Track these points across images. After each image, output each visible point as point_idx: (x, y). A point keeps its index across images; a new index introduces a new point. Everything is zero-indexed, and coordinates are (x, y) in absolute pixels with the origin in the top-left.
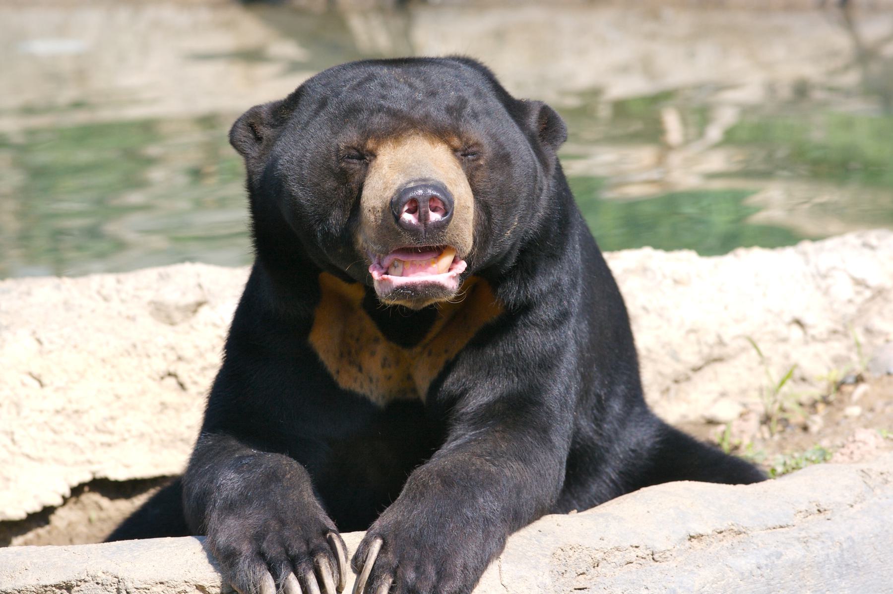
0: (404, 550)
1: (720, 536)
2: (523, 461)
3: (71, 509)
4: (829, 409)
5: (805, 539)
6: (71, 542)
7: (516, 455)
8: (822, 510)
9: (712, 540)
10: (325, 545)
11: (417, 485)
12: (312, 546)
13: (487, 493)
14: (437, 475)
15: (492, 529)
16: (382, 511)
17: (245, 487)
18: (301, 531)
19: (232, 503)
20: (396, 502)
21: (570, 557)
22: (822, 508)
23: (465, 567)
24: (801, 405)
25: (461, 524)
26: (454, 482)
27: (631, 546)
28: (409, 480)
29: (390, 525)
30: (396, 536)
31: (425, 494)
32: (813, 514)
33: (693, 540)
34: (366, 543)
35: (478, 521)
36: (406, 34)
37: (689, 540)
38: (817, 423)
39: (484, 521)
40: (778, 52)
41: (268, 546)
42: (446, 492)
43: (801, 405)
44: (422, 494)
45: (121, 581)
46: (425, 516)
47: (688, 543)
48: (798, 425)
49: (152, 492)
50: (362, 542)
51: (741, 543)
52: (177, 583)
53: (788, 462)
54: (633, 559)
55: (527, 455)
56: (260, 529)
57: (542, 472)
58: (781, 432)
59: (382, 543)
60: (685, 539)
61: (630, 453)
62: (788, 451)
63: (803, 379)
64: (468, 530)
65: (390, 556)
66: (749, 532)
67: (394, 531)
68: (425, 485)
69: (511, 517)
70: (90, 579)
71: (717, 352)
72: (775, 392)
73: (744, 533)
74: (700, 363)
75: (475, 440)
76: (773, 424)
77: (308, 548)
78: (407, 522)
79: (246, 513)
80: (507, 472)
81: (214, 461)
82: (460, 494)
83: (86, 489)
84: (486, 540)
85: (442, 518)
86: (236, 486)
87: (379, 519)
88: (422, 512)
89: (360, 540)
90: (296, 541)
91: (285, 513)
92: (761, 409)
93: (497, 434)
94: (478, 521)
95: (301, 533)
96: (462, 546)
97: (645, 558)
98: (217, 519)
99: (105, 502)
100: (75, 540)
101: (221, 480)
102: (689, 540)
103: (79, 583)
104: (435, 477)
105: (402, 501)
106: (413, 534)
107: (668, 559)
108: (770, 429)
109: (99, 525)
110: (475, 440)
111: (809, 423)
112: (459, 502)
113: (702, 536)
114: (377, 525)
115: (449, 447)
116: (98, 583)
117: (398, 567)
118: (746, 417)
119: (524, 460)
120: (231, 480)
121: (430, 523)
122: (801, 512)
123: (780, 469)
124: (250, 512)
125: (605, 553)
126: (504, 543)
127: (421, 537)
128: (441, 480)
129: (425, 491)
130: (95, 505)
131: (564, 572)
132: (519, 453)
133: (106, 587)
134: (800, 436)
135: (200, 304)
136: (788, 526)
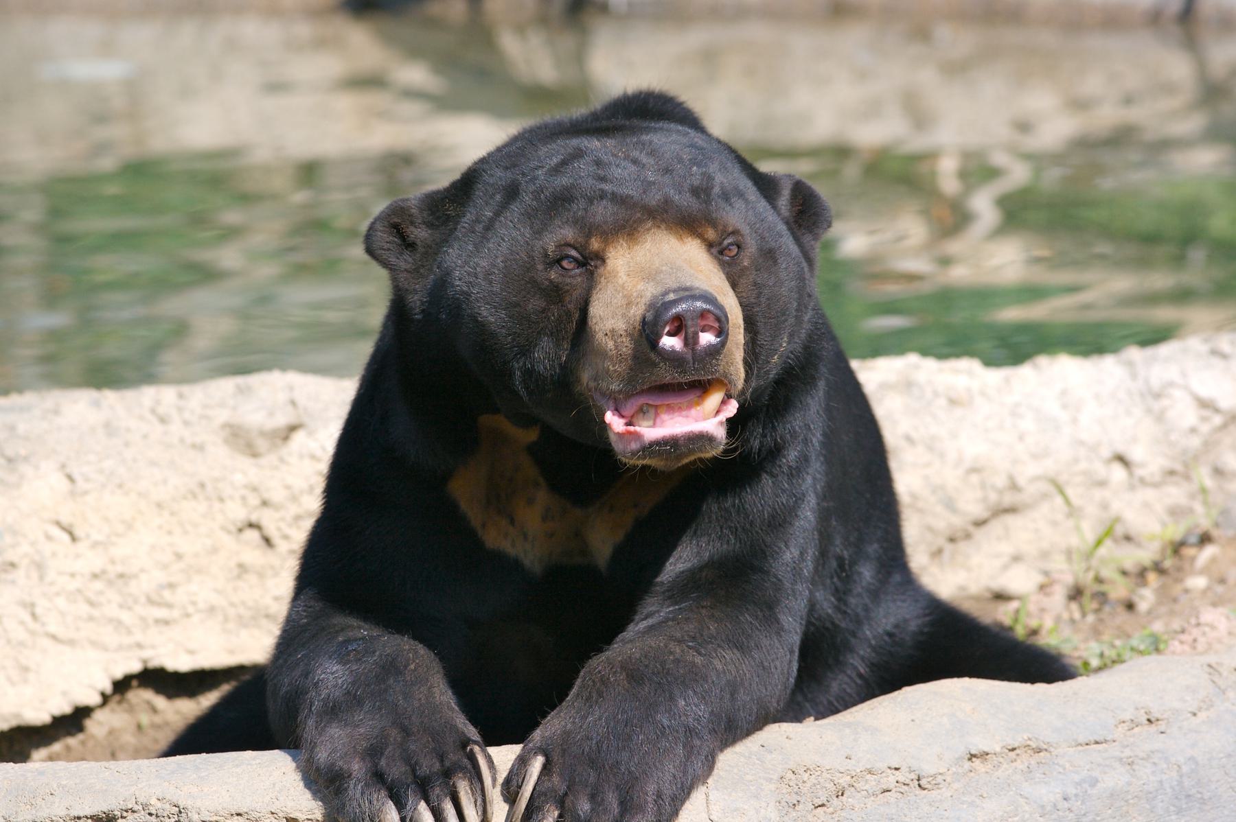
1: (1012, 754)
3: (113, 711)
4: (1164, 579)
6: (113, 756)
7: (729, 640)
8: (1153, 719)
9: (1001, 760)
11: (594, 681)
12: (447, 764)
14: (622, 667)
15: (697, 742)
16: (544, 717)
17: (353, 683)
19: (335, 706)
20: (564, 704)
21: (804, 782)
22: (1154, 717)
23: (659, 795)
24: (1124, 573)
26: (645, 678)
28: (582, 674)
30: (564, 751)
31: (605, 694)
32: (1141, 725)
33: (974, 759)
34: (522, 762)
35: (677, 732)
36: (579, 57)
37: (970, 759)
38: (1146, 598)
41: (388, 765)
43: (1124, 573)
44: (600, 695)
45: (183, 811)
47: (967, 765)
48: (1119, 601)
49: (226, 688)
50: (516, 759)
51: (1041, 765)
52: (262, 814)
54: (892, 785)
58: (1097, 611)
59: (544, 761)
61: (886, 638)
62: (1106, 638)
63: (1128, 538)
64: (664, 743)
65: (556, 779)
66: (1052, 749)
68: (604, 681)
69: (723, 727)
70: (141, 809)
71: (1008, 499)
72: (1089, 555)
73: (1046, 750)
74: (985, 515)
75: (673, 620)
76: (1086, 600)
79: (355, 719)
83: (135, 683)
84: (688, 757)
85: (628, 728)
86: (340, 681)
87: (540, 727)
88: (600, 719)
89: (514, 757)
92: (1069, 579)
93: (704, 611)
94: (677, 732)
96: (655, 766)
97: (908, 785)
99: (160, 701)
101: (319, 675)
102: (970, 759)
103: (125, 814)
104: (618, 669)
105: (573, 703)
106: (587, 749)
107: (941, 786)
109: (152, 733)
111: (1136, 599)
113: (987, 754)
114: (537, 735)
115: (636, 629)
116: (150, 814)
117: (566, 794)
118: (1048, 590)
119: (740, 647)
122: (1124, 722)
123: (1095, 662)
125: (853, 777)
126: (714, 762)
127: (599, 752)
128: (627, 675)
131: (796, 802)
133: (162, 819)
134: (1123, 616)
135: (293, 428)
136: (1106, 741)
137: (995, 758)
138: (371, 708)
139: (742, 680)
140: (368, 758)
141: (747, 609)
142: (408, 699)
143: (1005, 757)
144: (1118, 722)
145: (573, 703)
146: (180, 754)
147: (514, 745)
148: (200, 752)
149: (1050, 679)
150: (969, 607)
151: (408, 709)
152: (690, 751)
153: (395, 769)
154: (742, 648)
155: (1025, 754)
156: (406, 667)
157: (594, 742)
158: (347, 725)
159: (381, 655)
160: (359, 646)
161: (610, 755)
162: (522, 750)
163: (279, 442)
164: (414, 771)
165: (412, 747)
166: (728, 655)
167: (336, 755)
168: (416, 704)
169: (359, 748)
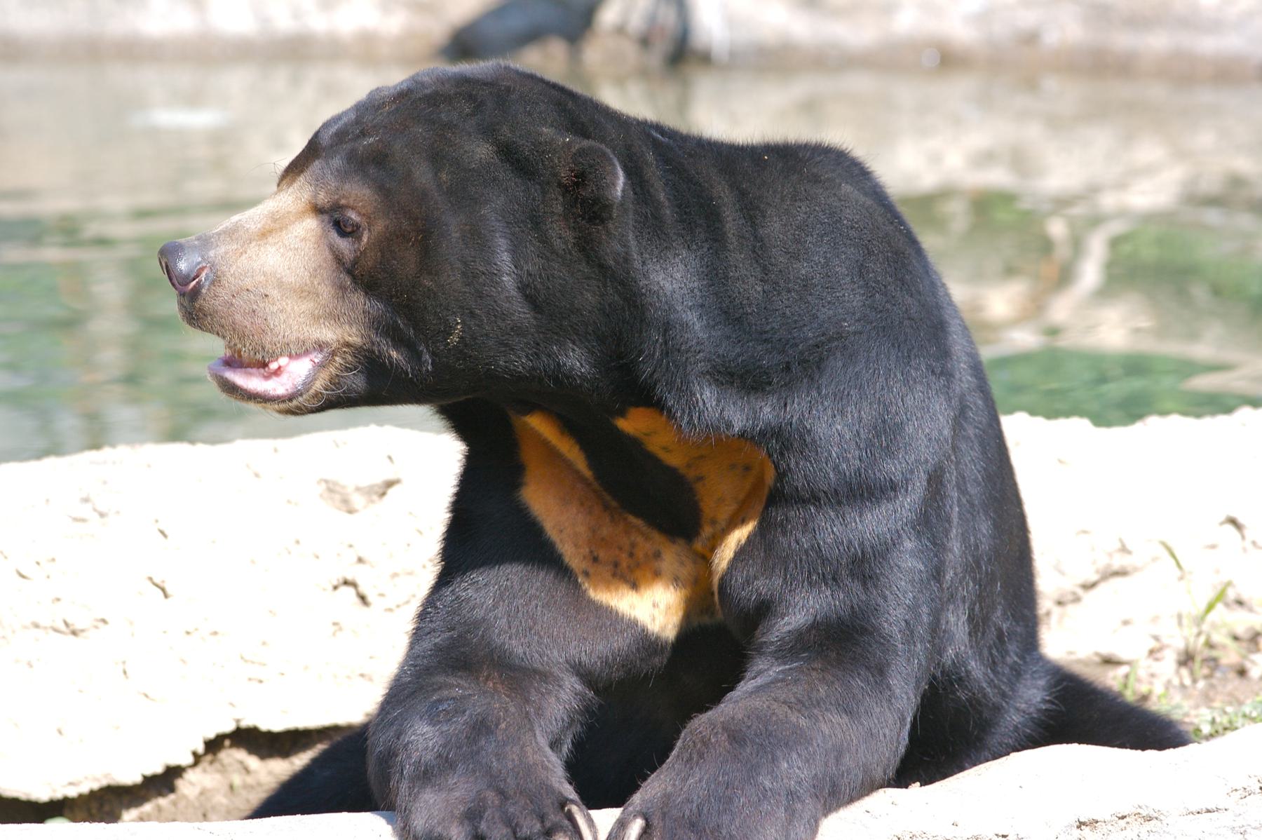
0: (675, 835)
1: (1122, 822)
2: (849, 714)
3: (205, 771)
5: (1242, 830)
6: (205, 817)
7: (839, 705)
9: (1110, 827)
10: (566, 822)
11: (694, 742)
12: (548, 824)
13: (795, 756)
14: (723, 728)
15: (799, 806)
16: (645, 779)
17: (445, 746)
18: (530, 804)
19: (427, 770)
20: (664, 765)
24: (1236, 638)
25: (756, 799)
26: (747, 739)
27: (997, 835)
28: (683, 735)
29: (655, 799)
30: (664, 814)
31: (705, 755)
32: (1254, 793)
33: (1083, 827)
34: (622, 825)
35: (779, 794)
36: (683, 104)
37: (1079, 827)
39: (787, 795)
40: (1205, 139)
41: (488, 827)
42: (735, 751)
43: (1236, 638)
44: (701, 756)
46: (705, 786)
47: (1077, 832)
48: (1231, 667)
49: (320, 747)
50: (616, 823)
51: (1152, 834)
53: (1218, 720)
55: (854, 705)
56: (472, 804)
57: (873, 731)
58: (1206, 677)
59: (644, 825)
60: (1072, 826)
62: (1217, 704)
63: (1240, 603)
64: (765, 806)
66: (1162, 817)
67: (662, 808)
68: (706, 743)
69: (827, 791)
71: (1118, 562)
72: (1200, 620)
73: (1157, 818)
74: (1094, 578)
75: (782, 680)
76: (1197, 665)
77: (543, 826)
78: (679, 795)
79: (449, 782)
80: (825, 728)
81: (405, 705)
82: (754, 756)
83: (227, 743)
84: (790, 822)
85: (729, 790)
86: (430, 744)
87: (641, 790)
88: (700, 781)
89: (614, 820)
90: (525, 818)
91: (505, 780)
92: (1181, 645)
93: (814, 674)
95: (531, 807)
96: (756, 829)
98: (407, 794)
99: (253, 762)
100: (209, 815)
101: (409, 737)
102: (1079, 827)
104: (720, 731)
105: (673, 765)
106: (687, 813)
108: (1192, 673)
109: (244, 793)
110: (782, 680)
111: (1248, 665)
112: (752, 766)
113: (1097, 822)
114: (637, 798)
115: (745, 688)
118: (1158, 655)
119: (849, 712)
120: (422, 735)
121: (711, 798)
122: (1236, 790)
123: (1206, 729)
124: (454, 782)
126: (817, 826)
127: (700, 816)
128: (729, 736)
129: (706, 750)
130: (239, 766)
132: (843, 702)
134: (1234, 683)
135: (390, 484)
136: (1218, 810)
137: (1104, 827)
138: (464, 771)
139: (849, 744)
140: (466, 822)
141: (859, 674)
142: (501, 760)
143: (1115, 824)
144: (1231, 790)
145: (673, 765)
146: (275, 815)
147: (614, 809)
148: (295, 814)
149: (1161, 746)
150: (1078, 669)
151: (502, 772)
152: (791, 813)
153: (496, 831)
154: (851, 713)
155: (1136, 822)
156: (497, 725)
157: (695, 805)
158: (442, 790)
159: (471, 716)
160: (449, 706)
161: (711, 819)
162: (622, 814)
163: (375, 497)
164: (515, 833)
165: (511, 810)
166: (836, 719)
167: (433, 821)
168: (510, 765)
169: (457, 812)
